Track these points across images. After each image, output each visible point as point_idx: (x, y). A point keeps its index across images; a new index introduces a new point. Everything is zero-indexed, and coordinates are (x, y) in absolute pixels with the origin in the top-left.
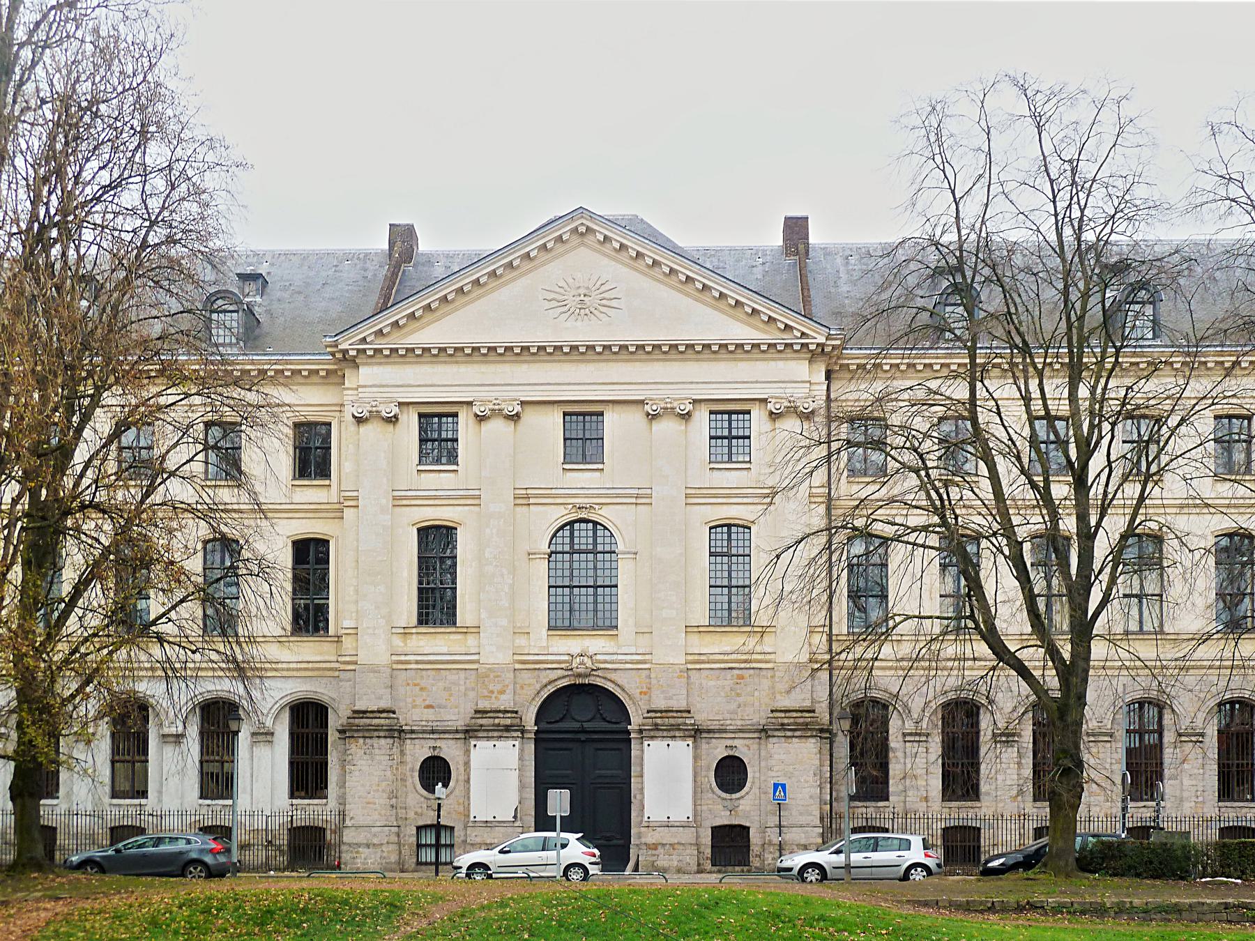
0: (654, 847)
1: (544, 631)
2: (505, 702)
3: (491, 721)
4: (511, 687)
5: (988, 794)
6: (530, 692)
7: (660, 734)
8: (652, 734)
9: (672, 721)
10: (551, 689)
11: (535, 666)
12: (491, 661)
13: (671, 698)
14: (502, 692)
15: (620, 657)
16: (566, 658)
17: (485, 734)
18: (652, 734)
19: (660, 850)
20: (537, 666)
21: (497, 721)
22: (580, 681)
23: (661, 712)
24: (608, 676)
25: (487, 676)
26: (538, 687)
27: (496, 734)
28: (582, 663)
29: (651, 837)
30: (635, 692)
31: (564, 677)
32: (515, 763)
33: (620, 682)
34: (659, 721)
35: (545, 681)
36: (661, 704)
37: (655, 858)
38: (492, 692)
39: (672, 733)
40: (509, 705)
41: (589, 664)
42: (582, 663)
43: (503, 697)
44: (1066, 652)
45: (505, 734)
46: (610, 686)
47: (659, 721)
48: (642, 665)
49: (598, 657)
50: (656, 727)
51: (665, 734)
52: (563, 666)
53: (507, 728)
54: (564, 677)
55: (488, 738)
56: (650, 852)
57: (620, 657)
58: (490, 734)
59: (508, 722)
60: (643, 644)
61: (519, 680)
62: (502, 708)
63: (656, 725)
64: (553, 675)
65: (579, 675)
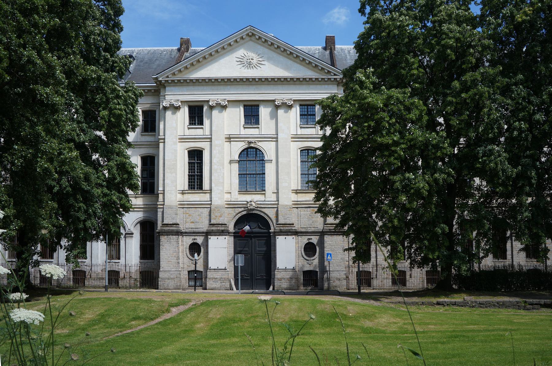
1: (237, 193)
21: (218, 228)
23: (283, 224)
26: (235, 214)
38: (216, 216)
41: (254, 205)
47: (282, 228)
55: (215, 235)
62: (221, 223)
63: (281, 230)
64: (240, 210)
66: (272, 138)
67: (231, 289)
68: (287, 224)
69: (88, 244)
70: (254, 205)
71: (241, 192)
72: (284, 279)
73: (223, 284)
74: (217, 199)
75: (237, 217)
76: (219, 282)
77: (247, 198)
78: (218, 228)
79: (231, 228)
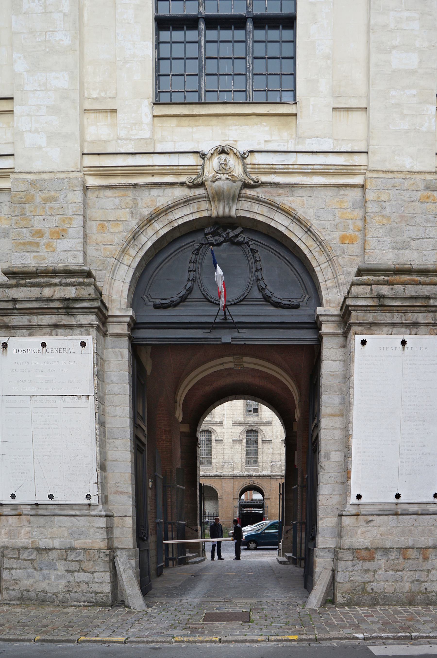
0: (368, 554)
1: (146, 109)
2: (66, 253)
3: (35, 292)
4: (78, 221)
5: (328, 302)
6: (118, 236)
7: (387, 317)
8: (370, 317)
9: (411, 290)
10: (160, 228)
11: (126, 179)
12: (37, 166)
13: (405, 246)
14: (61, 233)
15: (303, 159)
16: (191, 160)
17: (24, 320)
18: (370, 317)
19: (380, 561)
20: (133, 181)
21: (47, 292)
22: (219, 210)
23: (386, 272)
24: (279, 200)
25: (30, 200)
26: (133, 224)
27: (46, 320)
28: (224, 168)
29: (361, 536)
30: (331, 236)
31: (187, 201)
32: (86, 383)
33: (300, 213)
34: (385, 290)
35: (146, 212)
36: (385, 256)
37: (368, 577)
38: (40, 234)
39: (411, 317)
40: (74, 261)
41: (237, 168)
42: (224, 168)
43: (64, 244)
44: (226, 309)
45: (65, 320)
46: (280, 223)
47: (385, 290)
48: (344, 176)
49: (258, 159)
50: (381, 304)
51: (397, 318)
52: (183, 179)
53: (68, 307)
54: (187, 201)
55: (32, 329)
56: (360, 565)
57: (303, 159)
58: (35, 320)
59: (71, 292)
60: (350, 132)
61: (95, 213)
62: (60, 266)
63: (381, 297)
64: (164, 198)
65: (218, 196)
66: (203, 197)
67: (117, 600)
68: (409, 271)
69: (201, 481)
70: (237, 168)
71: (172, 91)
72: (386, 550)
73: (81, 577)
74: (42, 140)
75: (148, 239)
76: (61, 566)
77: (204, 135)
78: (47, 292)
79: (118, 293)
